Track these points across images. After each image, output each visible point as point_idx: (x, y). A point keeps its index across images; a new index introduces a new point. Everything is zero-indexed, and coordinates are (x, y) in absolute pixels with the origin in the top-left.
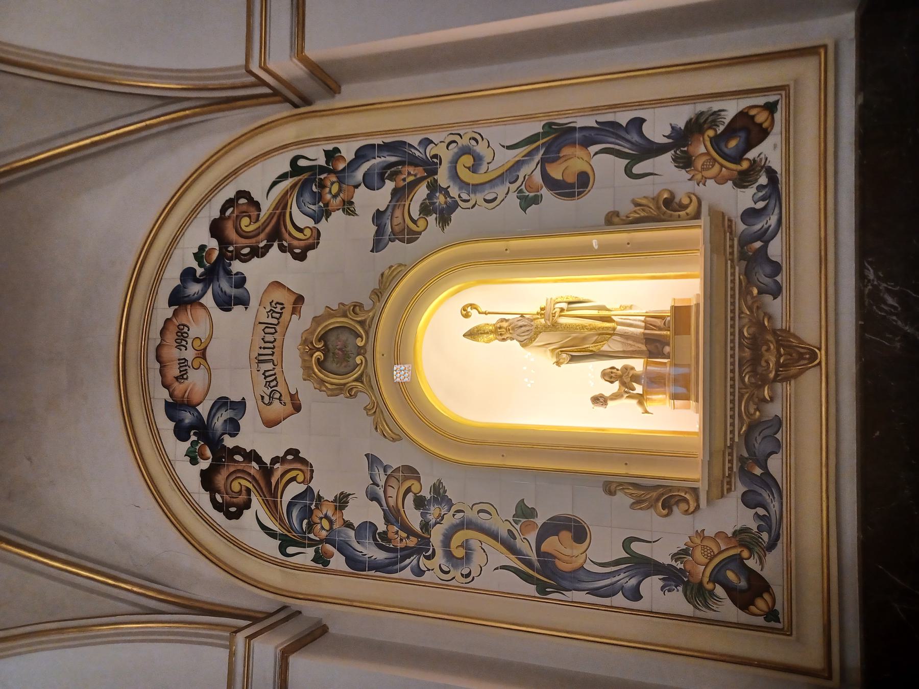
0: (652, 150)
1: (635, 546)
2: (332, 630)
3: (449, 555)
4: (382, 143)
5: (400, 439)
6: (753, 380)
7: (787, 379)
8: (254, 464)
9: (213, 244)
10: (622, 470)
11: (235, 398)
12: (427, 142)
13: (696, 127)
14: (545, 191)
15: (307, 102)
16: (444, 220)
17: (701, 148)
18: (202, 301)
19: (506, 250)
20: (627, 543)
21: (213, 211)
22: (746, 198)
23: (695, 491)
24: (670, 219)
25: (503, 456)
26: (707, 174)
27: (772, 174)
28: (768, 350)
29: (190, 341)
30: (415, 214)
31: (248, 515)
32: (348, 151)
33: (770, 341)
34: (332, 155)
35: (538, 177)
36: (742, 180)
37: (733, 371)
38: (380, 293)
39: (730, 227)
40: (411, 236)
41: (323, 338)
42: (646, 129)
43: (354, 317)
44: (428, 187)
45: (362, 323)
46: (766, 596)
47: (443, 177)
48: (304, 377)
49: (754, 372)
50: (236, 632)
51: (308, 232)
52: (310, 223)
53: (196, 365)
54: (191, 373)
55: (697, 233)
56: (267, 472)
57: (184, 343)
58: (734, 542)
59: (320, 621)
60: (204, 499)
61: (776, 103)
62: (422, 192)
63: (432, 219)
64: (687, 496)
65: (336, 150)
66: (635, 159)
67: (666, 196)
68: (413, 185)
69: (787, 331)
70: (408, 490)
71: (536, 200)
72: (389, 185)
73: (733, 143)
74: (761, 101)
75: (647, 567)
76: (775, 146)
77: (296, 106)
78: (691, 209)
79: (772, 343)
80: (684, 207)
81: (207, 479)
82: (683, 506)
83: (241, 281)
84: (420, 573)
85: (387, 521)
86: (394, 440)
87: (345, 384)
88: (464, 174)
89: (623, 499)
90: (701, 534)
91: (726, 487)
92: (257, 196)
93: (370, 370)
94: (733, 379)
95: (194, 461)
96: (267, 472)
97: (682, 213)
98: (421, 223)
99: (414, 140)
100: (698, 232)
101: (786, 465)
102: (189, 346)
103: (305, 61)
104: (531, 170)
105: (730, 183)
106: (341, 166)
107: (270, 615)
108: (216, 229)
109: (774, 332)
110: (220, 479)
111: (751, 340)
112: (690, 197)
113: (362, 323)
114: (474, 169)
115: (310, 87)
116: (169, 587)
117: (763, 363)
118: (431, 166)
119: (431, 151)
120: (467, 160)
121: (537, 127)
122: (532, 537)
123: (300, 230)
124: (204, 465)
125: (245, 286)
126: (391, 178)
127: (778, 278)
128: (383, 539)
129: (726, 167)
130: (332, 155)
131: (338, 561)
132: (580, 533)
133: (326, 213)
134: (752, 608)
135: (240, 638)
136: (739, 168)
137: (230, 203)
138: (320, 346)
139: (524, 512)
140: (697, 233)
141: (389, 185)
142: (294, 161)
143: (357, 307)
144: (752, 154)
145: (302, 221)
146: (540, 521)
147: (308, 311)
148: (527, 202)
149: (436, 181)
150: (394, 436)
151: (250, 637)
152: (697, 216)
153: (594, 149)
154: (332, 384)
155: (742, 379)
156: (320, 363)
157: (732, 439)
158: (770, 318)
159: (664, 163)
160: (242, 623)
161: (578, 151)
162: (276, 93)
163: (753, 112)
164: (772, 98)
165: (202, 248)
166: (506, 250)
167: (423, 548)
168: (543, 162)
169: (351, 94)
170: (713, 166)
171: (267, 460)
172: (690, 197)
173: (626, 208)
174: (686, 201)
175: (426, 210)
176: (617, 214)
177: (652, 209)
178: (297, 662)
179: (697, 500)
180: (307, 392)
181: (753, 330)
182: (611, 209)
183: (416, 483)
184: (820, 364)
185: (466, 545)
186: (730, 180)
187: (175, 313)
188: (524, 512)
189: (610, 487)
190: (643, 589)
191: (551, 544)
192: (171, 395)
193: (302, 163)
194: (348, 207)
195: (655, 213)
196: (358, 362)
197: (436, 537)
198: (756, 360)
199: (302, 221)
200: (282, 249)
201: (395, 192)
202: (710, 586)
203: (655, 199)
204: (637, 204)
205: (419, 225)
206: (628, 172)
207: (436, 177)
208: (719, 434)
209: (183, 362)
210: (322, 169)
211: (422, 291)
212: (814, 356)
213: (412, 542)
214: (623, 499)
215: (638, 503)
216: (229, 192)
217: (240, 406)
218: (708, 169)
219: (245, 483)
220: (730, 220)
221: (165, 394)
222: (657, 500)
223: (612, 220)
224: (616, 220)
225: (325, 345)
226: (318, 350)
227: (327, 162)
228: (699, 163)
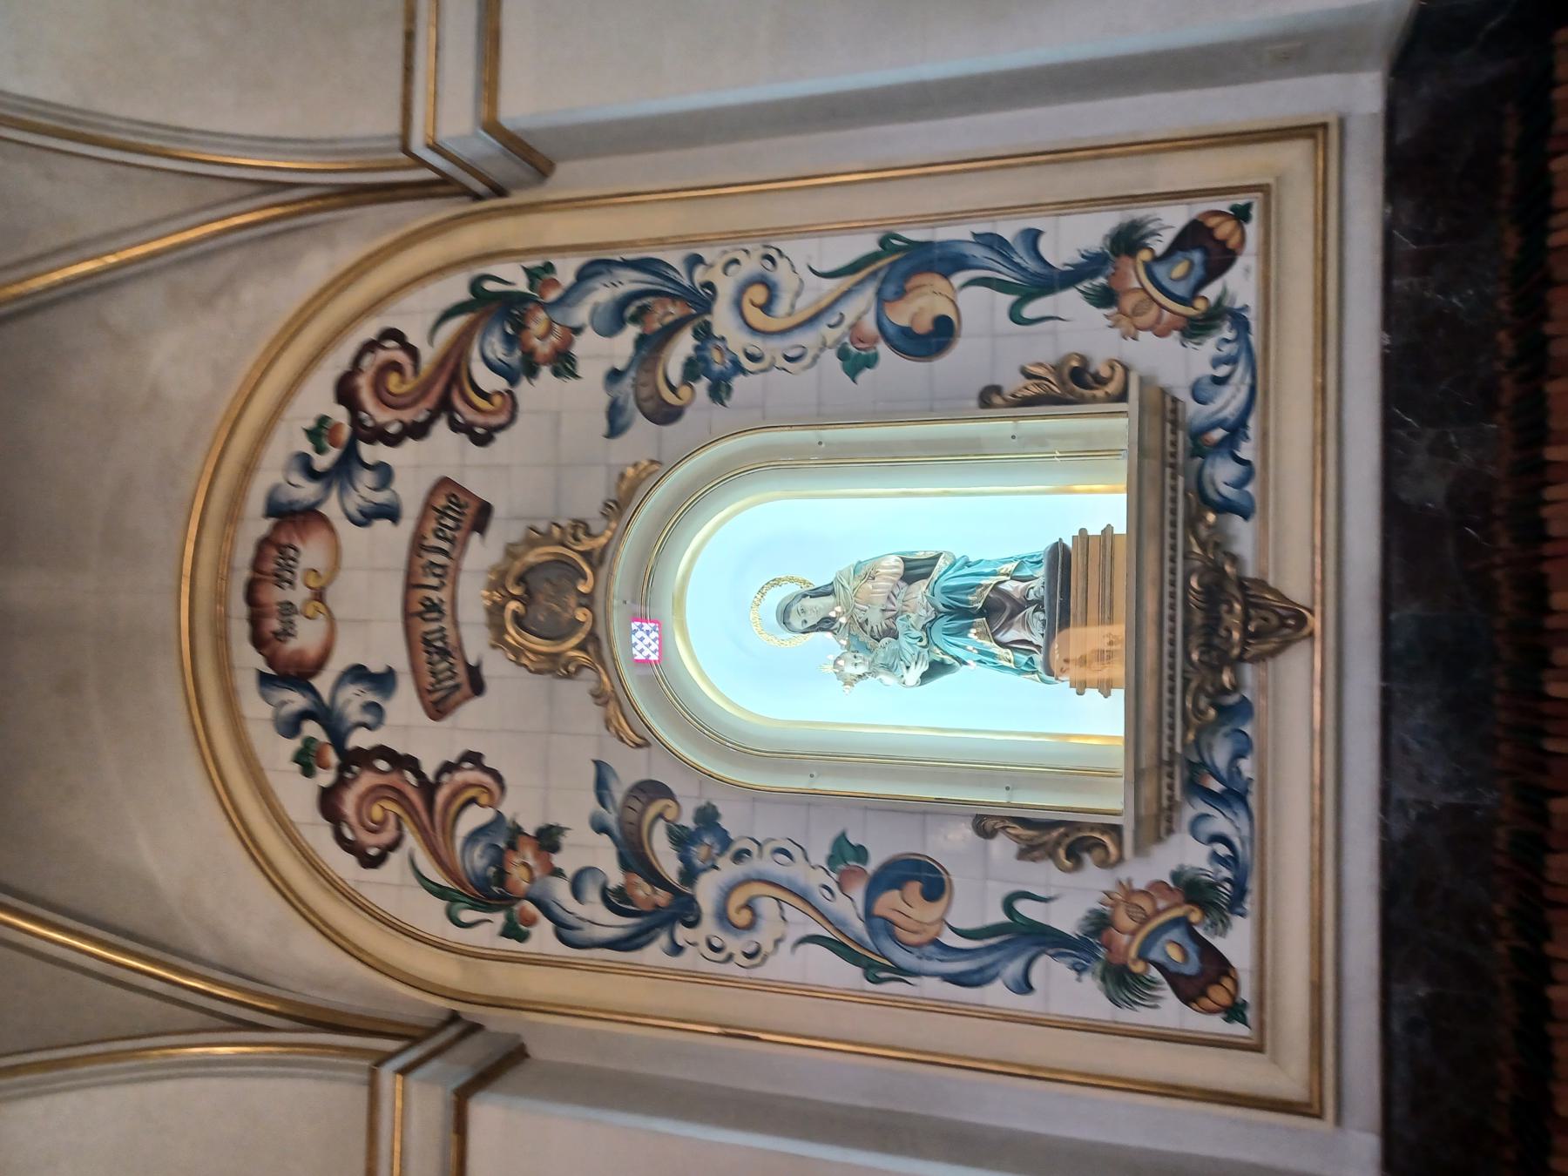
0: (1049, 281)
1: (1023, 907)
2: (534, 1049)
3: (723, 917)
4: (621, 260)
5: (647, 744)
6: (1206, 658)
7: (1259, 659)
8: (409, 775)
9: (340, 414)
10: (1002, 798)
11: (376, 666)
12: (695, 261)
13: (1127, 241)
14: (883, 348)
15: (499, 191)
16: (719, 391)
17: (1133, 276)
18: (323, 510)
19: (820, 443)
20: (1008, 905)
21: (340, 359)
22: (1201, 357)
23: (1115, 830)
24: (1081, 400)
25: (812, 776)
26: (1141, 321)
27: (1240, 322)
28: (1231, 611)
29: (299, 572)
30: (675, 374)
31: (396, 859)
32: (566, 270)
33: (1234, 596)
34: (540, 275)
35: (870, 324)
36: (1195, 329)
37: (1172, 642)
38: (618, 507)
39: (1174, 411)
40: (666, 415)
41: (520, 580)
42: (1044, 247)
43: (574, 544)
44: (696, 335)
45: (586, 555)
46: (1227, 983)
47: (722, 319)
48: (493, 642)
49: (1207, 647)
50: (379, 1063)
51: (497, 400)
52: (500, 383)
53: (310, 612)
54: (301, 623)
55: (1118, 427)
56: (428, 789)
57: (288, 575)
58: (1179, 897)
59: (518, 1036)
60: (320, 837)
61: (1248, 206)
62: (684, 345)
63: (702, 385)
64: (1106, 839)
65: (549, 268)
66: (1027, 296)
67: (1075, 364)
68: (670, 331)
69: (1262, 584)
70: (660, 816)
71: (871, 361)
72: (632, 331)
73: (1180, 270)
74: (1223, 205)
75: (1045, 939)
76: (1247, 270)
77: (477, 197)
78: (1112, 388)
79: (1237, 601)
80: (1101, 381)
81: (329, 803)
82: (1098, 852)
83: (384, 473)
84: (676, 950)
85: (625, 865)
86: (638, 746)
87: (558, 655)
88: (756, 317)
89: (1002, 848)
90: (1129, 892)
91: (1164, 825)
92: (414, 338)
93: (601, 632)
94: (1172, 655)
95: (308, 771)
96: (428, 789)
97: (1099, 393)
98: (684, 391)
99: (674, 258)
100: (1122, 422)
101: (1261, 768)
102: (299, 582)
103: (492, 127)
104: (861, 307)
105: (1176, 334)
106: (552, 295)
107: (431, 1032)
108: (345, 392)
109: (1241, 583)
110: (349, 803)
111: (1201, 596)
112: (1112, 368)
113: (586, 555)
114: (766, 308)
115: (502, 167)
116: (273, 986)
117: (1223, 633)
118: (701, 300)
119: (700, 275)
120: (759, 294)
121: (867, 244)
122: (858, 892)
123: (484, 396)
124: (326, 778)
125: (393, 487)
126: (635, 319)
127: (1250, 488)
128: (616, 901)
129: (1169, 310)
130: (540, 275)
131: (543, 937)
132: (934, 885)
133: (530, 368)
134: (1206, 1002)
135: (387, 1073)
136: (1190, 311)
137: (370, 346)
138: (516, 591)
139: (845, 854)
140: (1118, 427)
141: (632, 331)
142: (476, 285)
143: (581, 526)
144: (1211, 292)
145: (489, 381)
146: (872, 866)
147: (501, 532)
148: (855, 362)
149: (708, 325)
150: (638, 741)
151: (404, 1071)
152: (1122, 397)
153: (959, 278)
154: (535, 653)
155: (1187, 655)
156: (518, 619)
157: (1172, 750)
158: (1234, 559)
159: (1070, 301)
160: (390, 1045)
161: (939, 283)
162: (445, 180)
163: (1212, 222)
164: (1241, 200)
165: (323, 420)
166: (820, 443)
167: (684, 911)
168: (881, 299)
169: (570, 178)
170: (1149, 309)
171: (429, 769)
172: (1112, 368)
173: (1013, 383)
174: (1105, 372)
175: (692, 370)
176: (997, 390)
177: (1052, 383)
178: (486, 1113)
179: (1119, 844)
180: (496, 667)
181: (1207, 579)
182: (987, 382)
183: (670, 802)
184: (1311, 634)
185: (749, 906)
186: (1176, 329)
187: (276, 527)
188: (845, 854)
189: (985, 826)
190: (1036, 977)
191: (889, 902)
192: (271, 662)
193: (490, 286)
194: (564, 364)
195: (1059, 392)
196: (581, 618)
197: (706, 891)
198: (1213, 624)
199: (489, 381)
200: (455, 427)
201: (641, 342)
202: (1138, 968)
203: (1057, 369)
204: (1029, 376)
205: (681, 396)
206: (1015, 316)
207: (707, 318)
208: (1149, 741)
209: (288, 609)
210: (522, 298)
211: (685, 509)
212: (1301, 621)
213: (662, 897)
214: (1002, 848)
215: (1028, 852)
216: (370, 329)
217: (384, 681)
218: (1143, 314)
219: (392, 807)
220: (1175, 400)
221: (258, 662)
222: (1058, 843)
223: (988, 397)
224: (997, 400)
225: (527, 591)
226: (515, 598)
227: (531, 287)
228: (1128, 303)
